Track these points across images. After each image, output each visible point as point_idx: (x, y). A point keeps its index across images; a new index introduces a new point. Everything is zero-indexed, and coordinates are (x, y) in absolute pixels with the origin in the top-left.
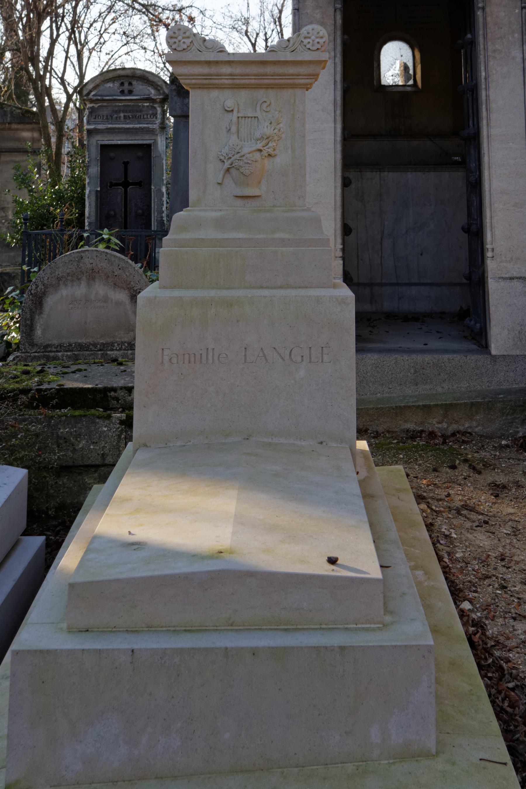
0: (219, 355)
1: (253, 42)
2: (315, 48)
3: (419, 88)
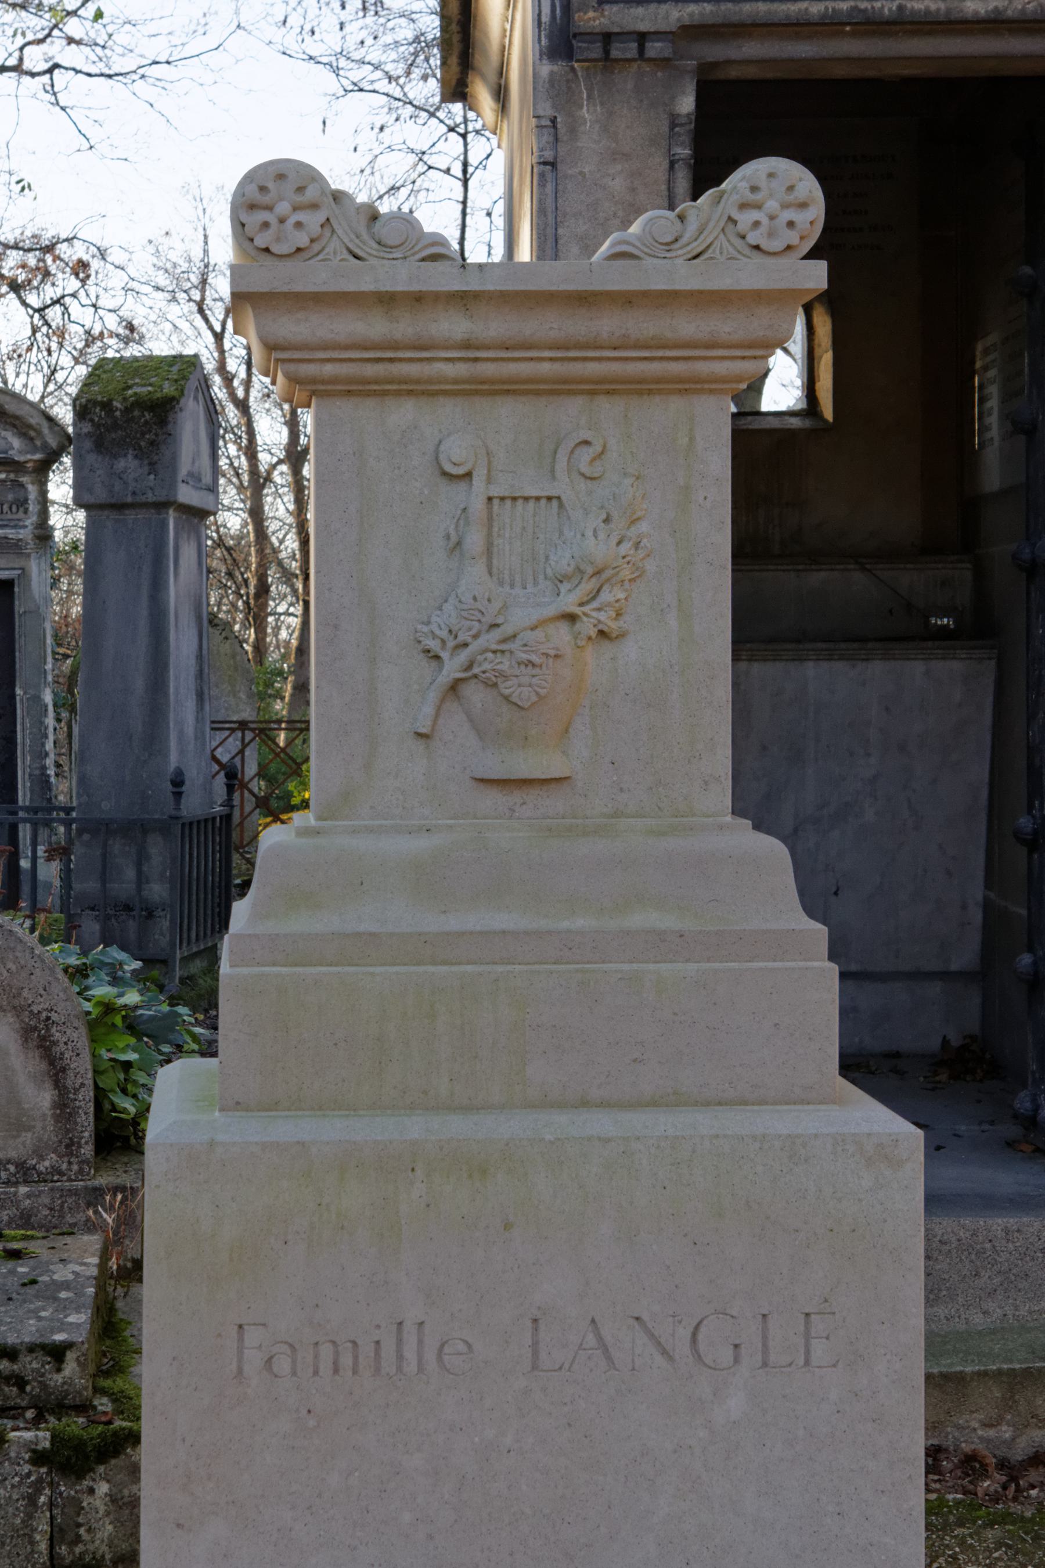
0: (442, 1346)
1: (218, 328)
2: (777, 245)
3: (826, 421)
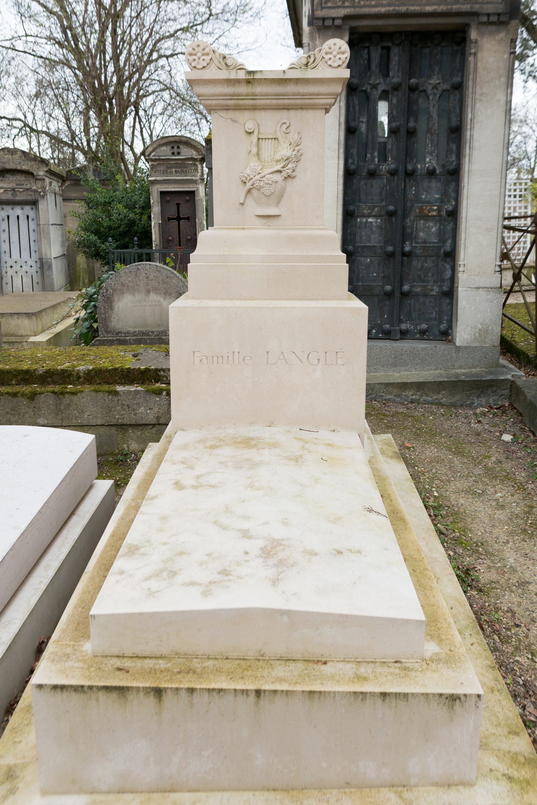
2: (336, 65)
